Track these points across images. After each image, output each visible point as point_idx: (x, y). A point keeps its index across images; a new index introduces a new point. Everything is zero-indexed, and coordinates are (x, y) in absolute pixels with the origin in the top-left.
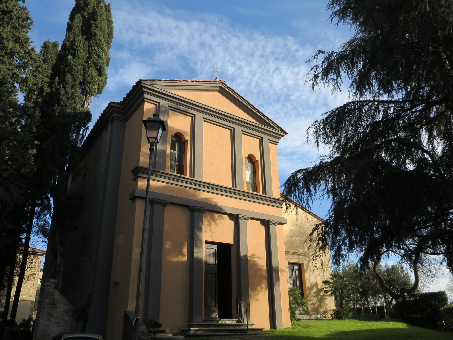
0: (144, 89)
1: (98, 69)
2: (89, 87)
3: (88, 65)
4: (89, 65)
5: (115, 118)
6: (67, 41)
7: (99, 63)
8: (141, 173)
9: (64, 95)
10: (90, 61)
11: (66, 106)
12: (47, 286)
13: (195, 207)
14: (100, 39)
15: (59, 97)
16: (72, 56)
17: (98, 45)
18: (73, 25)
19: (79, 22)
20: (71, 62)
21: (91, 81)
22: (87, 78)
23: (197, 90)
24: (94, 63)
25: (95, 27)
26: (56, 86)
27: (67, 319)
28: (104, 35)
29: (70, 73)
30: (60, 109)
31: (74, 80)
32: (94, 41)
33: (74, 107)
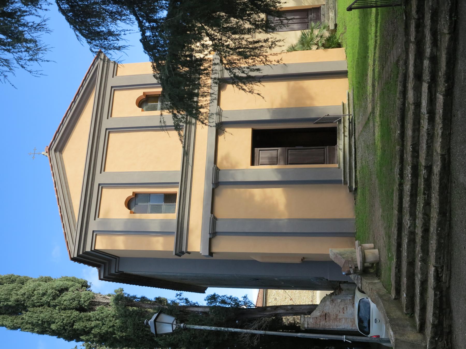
0: (81, 253)
1: (59, 293)
2: (85, 302)
4: (58, 304)
5: (117, 271)
6: (33, 330)
7: (52, 293)
8: (181, 249)
9: (100, 329)
10: (52, 304)
11: (114, 326)
12: (308, 324)
13: (213, 182)
14: (22, 295)
15: (104, 333)
16: (52, 325)
17: (31, 296)
18: (12, 326)
19: (5, 320)
20: (59, 325)
21: (77, 300)
22: (74, 305)
23: (66, 183)
24: (54, 299)
25: (8, 301)
26: (91, 338)
27: (339, 301)
28: (15, 289)
31: (81, 319)
32: (26, 301)
33: (113, 317)
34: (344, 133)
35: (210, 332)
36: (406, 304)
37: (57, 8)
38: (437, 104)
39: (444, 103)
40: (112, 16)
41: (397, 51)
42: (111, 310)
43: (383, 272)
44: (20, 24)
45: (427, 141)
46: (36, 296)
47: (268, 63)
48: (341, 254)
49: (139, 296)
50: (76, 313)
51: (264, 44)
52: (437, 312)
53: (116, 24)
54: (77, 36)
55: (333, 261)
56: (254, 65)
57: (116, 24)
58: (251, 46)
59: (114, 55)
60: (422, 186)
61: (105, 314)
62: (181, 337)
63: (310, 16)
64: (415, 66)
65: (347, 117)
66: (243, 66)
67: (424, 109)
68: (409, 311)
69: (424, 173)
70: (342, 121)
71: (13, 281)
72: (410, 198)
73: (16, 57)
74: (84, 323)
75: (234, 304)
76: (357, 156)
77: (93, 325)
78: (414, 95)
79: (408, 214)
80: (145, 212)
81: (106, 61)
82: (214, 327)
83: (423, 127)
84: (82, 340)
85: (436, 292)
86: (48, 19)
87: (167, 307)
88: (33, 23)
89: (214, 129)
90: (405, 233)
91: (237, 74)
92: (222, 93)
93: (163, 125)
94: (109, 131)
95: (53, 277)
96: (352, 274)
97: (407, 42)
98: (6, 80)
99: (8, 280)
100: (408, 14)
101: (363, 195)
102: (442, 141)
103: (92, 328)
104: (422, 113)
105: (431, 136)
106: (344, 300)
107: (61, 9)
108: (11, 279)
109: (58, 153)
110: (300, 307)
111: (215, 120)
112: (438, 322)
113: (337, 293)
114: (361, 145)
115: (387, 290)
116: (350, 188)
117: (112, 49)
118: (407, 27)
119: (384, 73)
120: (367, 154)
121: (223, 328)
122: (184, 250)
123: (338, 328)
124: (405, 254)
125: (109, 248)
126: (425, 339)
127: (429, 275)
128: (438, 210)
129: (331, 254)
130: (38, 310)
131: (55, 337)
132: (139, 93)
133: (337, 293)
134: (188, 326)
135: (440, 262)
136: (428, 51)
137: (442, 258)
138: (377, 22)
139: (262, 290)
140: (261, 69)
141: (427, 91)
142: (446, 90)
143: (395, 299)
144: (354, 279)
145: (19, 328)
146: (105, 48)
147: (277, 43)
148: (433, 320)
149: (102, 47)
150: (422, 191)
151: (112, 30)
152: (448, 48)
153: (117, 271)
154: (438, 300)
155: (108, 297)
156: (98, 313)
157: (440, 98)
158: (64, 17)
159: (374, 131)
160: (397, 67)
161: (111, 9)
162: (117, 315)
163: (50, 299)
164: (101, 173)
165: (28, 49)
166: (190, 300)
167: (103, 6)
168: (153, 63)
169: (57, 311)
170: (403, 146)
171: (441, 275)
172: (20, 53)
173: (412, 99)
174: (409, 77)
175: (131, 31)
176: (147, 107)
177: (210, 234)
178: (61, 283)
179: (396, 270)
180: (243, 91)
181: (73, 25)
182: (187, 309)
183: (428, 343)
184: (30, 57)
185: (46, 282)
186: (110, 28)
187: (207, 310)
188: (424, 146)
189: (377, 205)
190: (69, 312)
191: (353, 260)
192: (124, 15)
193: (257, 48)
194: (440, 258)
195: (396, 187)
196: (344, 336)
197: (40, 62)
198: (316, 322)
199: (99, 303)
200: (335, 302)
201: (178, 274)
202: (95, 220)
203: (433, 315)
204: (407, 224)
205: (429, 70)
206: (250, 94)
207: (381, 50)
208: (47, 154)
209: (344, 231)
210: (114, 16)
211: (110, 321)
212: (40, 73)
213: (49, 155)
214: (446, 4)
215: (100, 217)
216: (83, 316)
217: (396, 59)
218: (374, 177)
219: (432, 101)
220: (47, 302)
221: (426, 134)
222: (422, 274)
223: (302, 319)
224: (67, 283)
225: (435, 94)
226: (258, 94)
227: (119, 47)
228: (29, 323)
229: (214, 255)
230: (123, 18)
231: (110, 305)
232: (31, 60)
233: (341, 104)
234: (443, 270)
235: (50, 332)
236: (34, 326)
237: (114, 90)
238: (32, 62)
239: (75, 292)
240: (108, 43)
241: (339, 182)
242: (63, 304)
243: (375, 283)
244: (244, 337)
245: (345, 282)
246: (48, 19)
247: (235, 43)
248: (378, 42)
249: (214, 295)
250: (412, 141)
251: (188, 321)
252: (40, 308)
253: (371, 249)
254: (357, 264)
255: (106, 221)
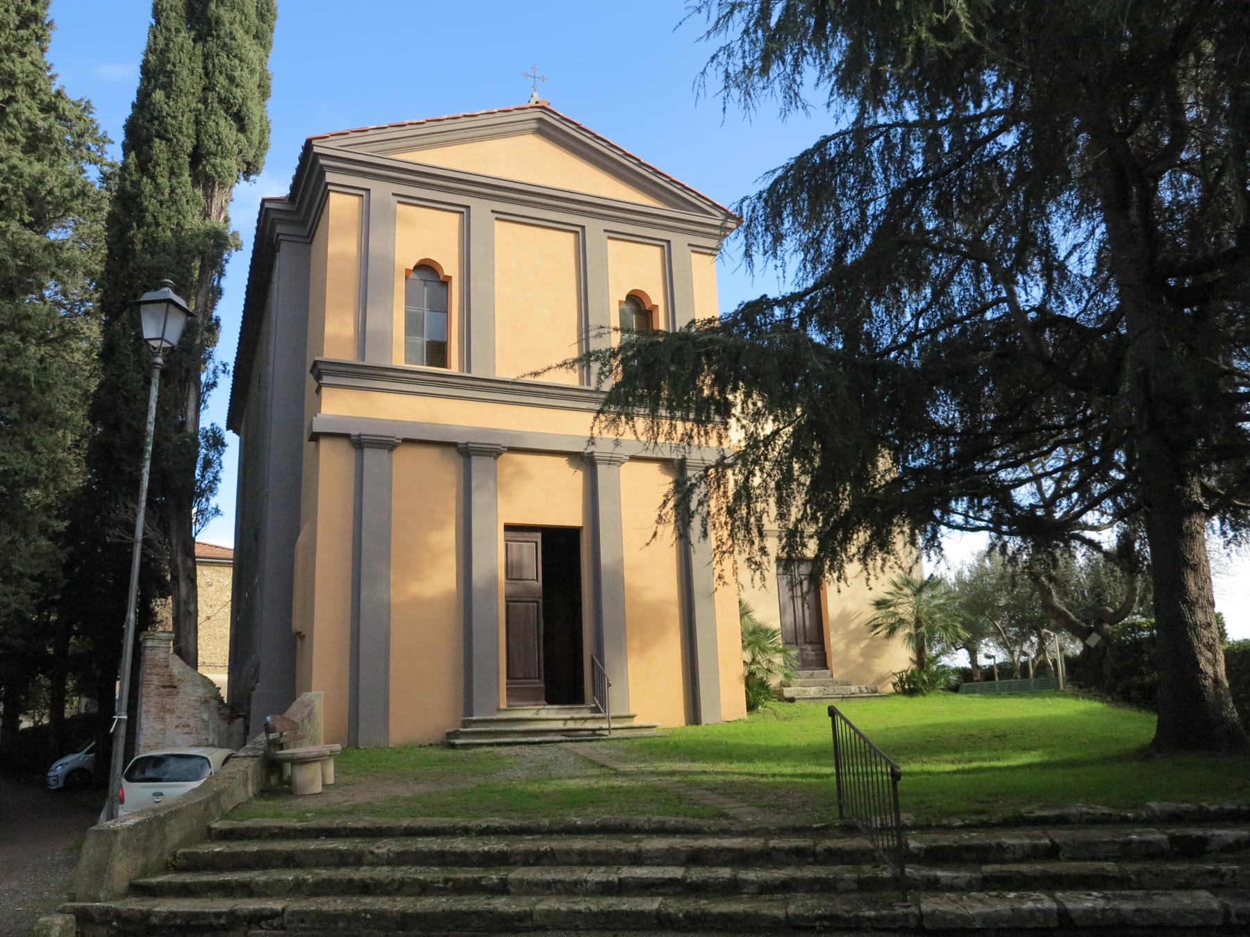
0: (322, 161)
2: (214, 166)
3: (206, 108)
5: (280, 237)
6: (151, 52)
9: (151, 196)
11: (158, 225)
12: (153, 648)
14: (231, 33)
15: (142, 203)
22: (206, 142)
23: (472, 139)
24: (221, 101)
27: (205, 716)
29: (161, 137)
30: (146, 234)
31: (175, 155)
33: (178, 224)
34: (572, 719)
35: (142, 433)
36: (196, 853)
37: (830, 133)
38: (638, 899)
39: (642, 912)
40: (812, 243)
41: (747, 815)
42: (193, 221)
43: (270, 803)
44: (798, 58)
45: (560, 881)
46: (228, 62)
47: (718, 556)
48: (310, 714)
49: (224, 283)
50: (188, 145)
51: (756, 547)
52: (178, 922)
53: (795, 251)
54: (774, 171)
55: (294, 700)
56: (714, 525)
57: (795, 251)
58: (752, 520)
59: (734, 244)
60: (462, 874)
61: (186, 207)
62: (128, 371)
63: (809, 647)
64: (718, 851)
65: (605, 726)
66: (713, 503)
67: (627, 872)
68: (182, 862)
69: (491, 879)
70: (597, 715)
71: (262, 16)
72: (437, 852)
73: (732, 45)
74: (165, 162)
75: (203, 486)
76: (523, 746)
77: (160, 180)
78: (658, 850)
79: (401, 849)
80: (409, 301)
81: (724, 232)
82: (153, 429)
83: (591, 871)
84: (126, 155)
85: (224, 917)
86: (807, 113)
87: (198, 342)
88: (801, 83)
89: (579, 448)
90: (359, 845)
91: (697, 491)
92: (655, 467)
93: (592, 333)
94: (580, 233)
95: (268, 102)
96: (268, 737)
97: (766, 833)
98: (691, 10)
99: (265, 6)
100: (824, 831)
101: (440, 760)
102: (561, 912)
103: (153, 178)
104: (619, 869)
105: (572, 889)
106: (206, 727)
107: (826, 140)
108: (265, 13)
109: (535, 125)
110: (192, 631)
111: (599, 450)
112: (154, 926)
113: (222, 711)
114: (548, 753)
115: (231, 811)
116: (456, 734)
117: (747, 240)
118: (797, 831)
119: (698, 792)
120: (528, 765)
121: (150, 448)
122: (326, 380)
123: (143, 715)
124: (313, 845)
125: (332, 222)
126: (116, 897)
127: (264, 900)
128: (410, 911)
129: (310, 694)
130: (195, 66)
131: (133, 97)
132: (656, 297)
133: (222, 711)
134: (155, 381)
135: (293, 921)
136: (750, 875)
137: (303, 925)
138: (803, 776)
139: (231, 554)
140: (707, 540)
141: (667, 876)
142: (669, 915)
143: (210, 829)
144: (255, 743)
145: (158, 22)
146: (749, 226)
147: (758, 572)
148: (159, 912)
149: (751, 221)
150: (452, 876)
151: (784, 242)
152: (757, 916)
153: (280, 237)
154: (205, 922)
155: (222, 216)
156: (189, 194)
157: (652, 904)
158: (811, 146)
159: (578, 777)
160: (715, 816)
161: (826, 242)
162: (183, 234)
163: (222, 91)
164: (493, 211)
165: (748, 71)
166: (214, 392)
167: (831, 226)
168: (719, 319)
169: (193, 105)
170: (549, 832)
171: (264, 926)
172: (740, 54)
173: (648, 847)
174: (695, 839)
175: (782, 279)
176: (629, 313)
177: (360, 435)
178: (256, 119)
179: (275, 828)
180: (661, 502)
181: (796, 162)
182: (192, 384)
183: (105, 904)
184: (732, 75)
185: (259, 86)
186: (788, 238)
187: (190, 429)
188: (550, 875)
189: (421, 788)
190: (191, 132)
191: (298, 740)
192: (815, 268)
193: (749, 533)
194: (303, 921)
195: (461, 821)
196: (126, 717)
197: (724, 93)
198: (158, 666)
199: (209, 197)
200: (203, 708)
201: (271, 369)
202: (394, 194)
203: (171, 913)
204: (378, 848)
205: (710, 878)
206: (656, 517)
207: (747, 785)
208: (533, 103)
209: (362, 724)
210: (812, 247)
211: (169, 219)
212: (701, 92)
213: (531, 107)
214: (846, 907)
215: (399, 207)
216: (180, 161)
217: (732, 812)
218: (481, 780)
219: (647, 888)
220: (215, 86)
221: (575, 877)
222: (267, 885)
223: (165, 635)
224: (257, 131)
225: (659, 894)
226: (655, 534)
227: (750, 256)
228: (167, 45)
229: (313, 443)
230: (809, 266)
231: (205, 219)
232: (727, 76)
233: (632, 712)
234: (275, 928)
235: (146, 87)
236: (161, 53)
237: (663, 246)
238: (723, 77)
239: (235, 147)
240: (758, 233)
241: (468, 709)
242: (209, 118)
243: (246, 786)
244: (126, 507)
245: (247, 727)
246: (807, 113)
247: (758, 487)
248: (762, 780)
249: (223, 445)
250: (559, 851)
251: (166, 386)
252: (201, 70)
253: (323, 776)
254: (288, 748)
255: (391, 218)
